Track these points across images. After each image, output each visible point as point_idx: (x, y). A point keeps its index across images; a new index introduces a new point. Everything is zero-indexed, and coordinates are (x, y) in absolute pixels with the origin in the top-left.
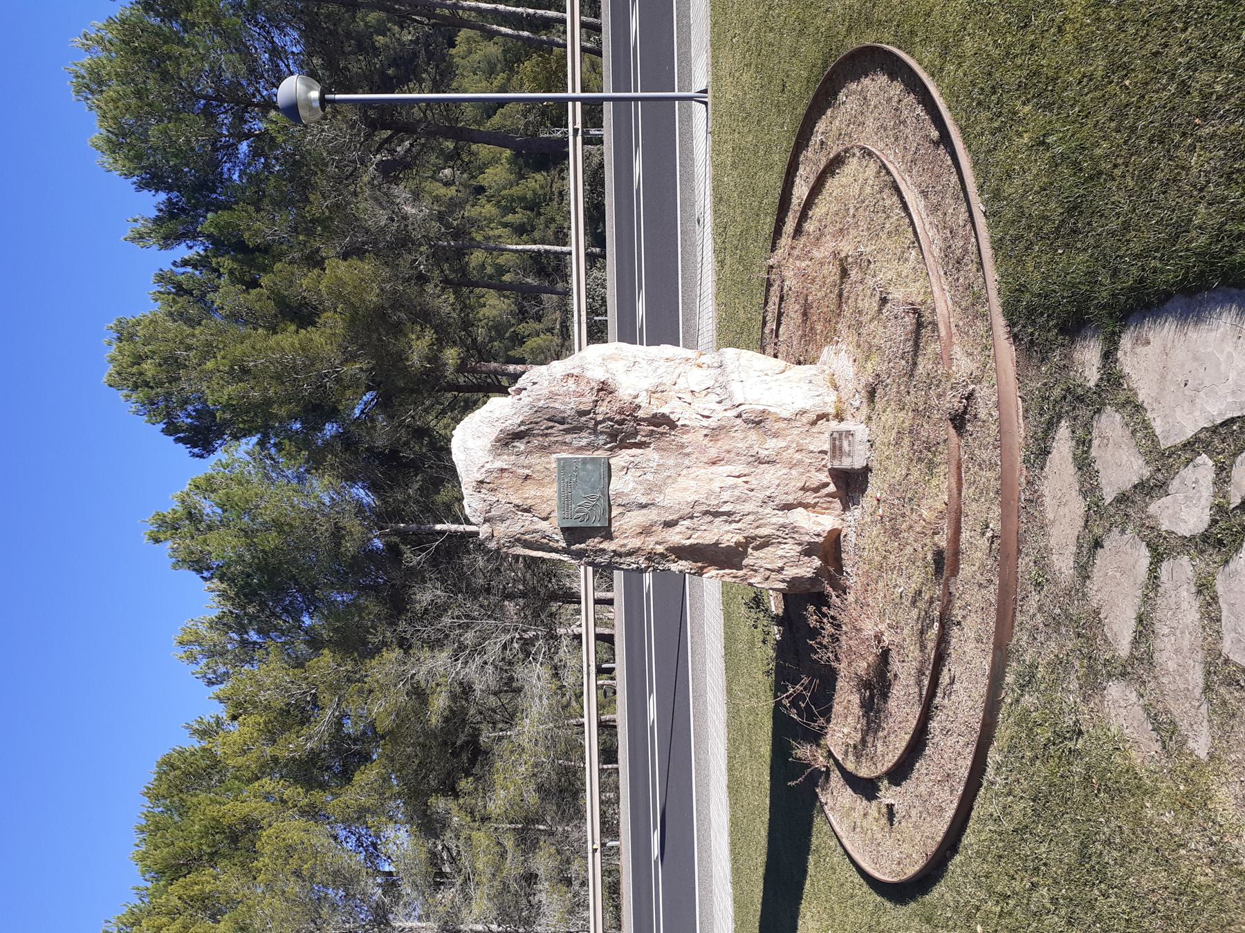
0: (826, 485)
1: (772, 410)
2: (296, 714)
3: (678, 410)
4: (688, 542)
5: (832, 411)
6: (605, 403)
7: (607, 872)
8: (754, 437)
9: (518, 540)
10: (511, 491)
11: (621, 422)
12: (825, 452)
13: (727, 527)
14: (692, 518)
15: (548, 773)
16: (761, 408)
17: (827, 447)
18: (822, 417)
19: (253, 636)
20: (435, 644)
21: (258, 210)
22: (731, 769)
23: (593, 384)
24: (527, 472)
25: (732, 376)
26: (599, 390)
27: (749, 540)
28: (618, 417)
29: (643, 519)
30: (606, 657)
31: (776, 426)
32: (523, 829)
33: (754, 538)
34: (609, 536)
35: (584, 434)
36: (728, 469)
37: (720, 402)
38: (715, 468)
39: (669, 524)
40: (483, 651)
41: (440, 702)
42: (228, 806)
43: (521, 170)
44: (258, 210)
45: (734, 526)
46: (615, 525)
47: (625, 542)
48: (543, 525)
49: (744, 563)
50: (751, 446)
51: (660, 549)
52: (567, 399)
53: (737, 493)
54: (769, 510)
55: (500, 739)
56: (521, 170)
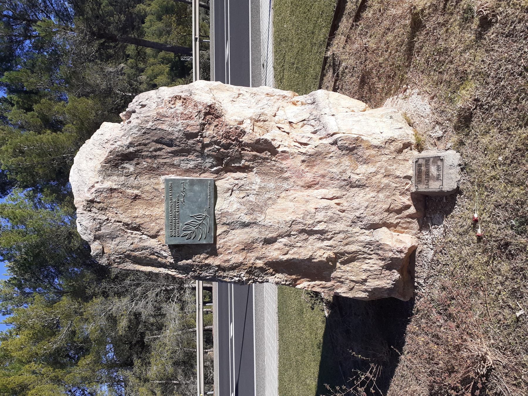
0: (408, 207)
1: (364, 138)
2: (52, 329)
3: (279, 138)
4: (285, 258)
5: (413, 141)
6: (212, 127)
7: (206, 313)
8: (347, 163)
9: (128, 256)
10: (120, 211)
11: (227, 147)
12: (408, 178)
13: (320, 244)
14: (289, 236)
15: (180, 355)
16: (356, 136)
17: (411, 172)
18: (407, 145)
19: (27, 290)
20: (119, 295)
21: (33, 72)
22: (281, 380)
23: (200, 107)
24: (136, 192)
25: (327, 111)
26: (206, 114)
27: (338, 255)
28: (224, 141)
29: (246, 236)
30: (207, 300)
31: (368, 152)
32: (166, 383)
33: (343, 254)
34: (213, 251)
35: (191, 157)
36: (323, 192)
37: (315, 133)
38: (310, 191)
39: (268, 242)
40: (146, 297)
41: (123, 323)
42: (12, 378)
43: (173, 77)
44: (33, 72)
45: (326, 243)
46: (220, 242)
47: (229, 257)
48: (152, 243)
49: (333, 275)
50: (344, 172)
51: (260, 263)
52: (175, 121)
53: (330, 213)
54: (357, 229)
55: (155, 339)
56: (173, 77)
